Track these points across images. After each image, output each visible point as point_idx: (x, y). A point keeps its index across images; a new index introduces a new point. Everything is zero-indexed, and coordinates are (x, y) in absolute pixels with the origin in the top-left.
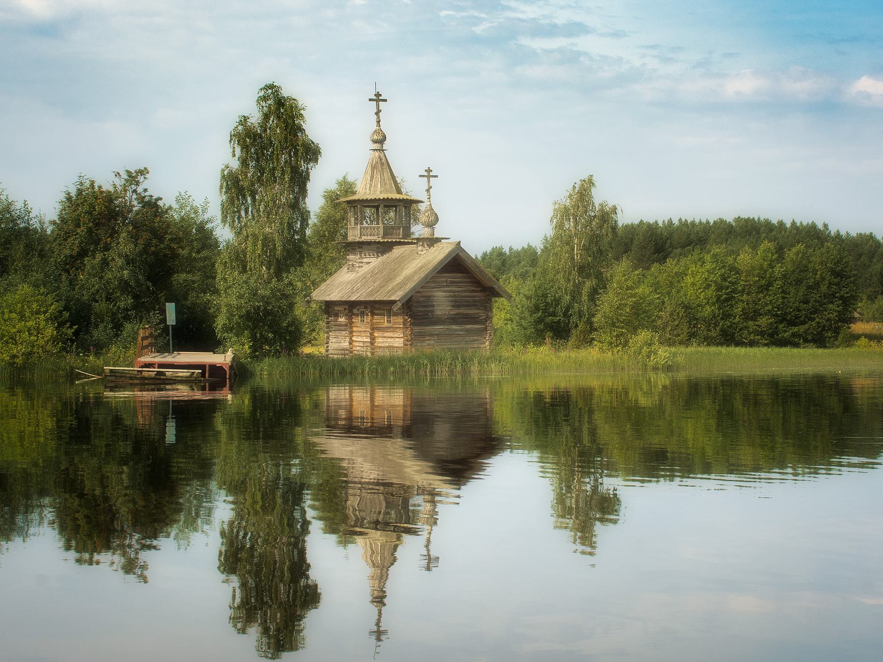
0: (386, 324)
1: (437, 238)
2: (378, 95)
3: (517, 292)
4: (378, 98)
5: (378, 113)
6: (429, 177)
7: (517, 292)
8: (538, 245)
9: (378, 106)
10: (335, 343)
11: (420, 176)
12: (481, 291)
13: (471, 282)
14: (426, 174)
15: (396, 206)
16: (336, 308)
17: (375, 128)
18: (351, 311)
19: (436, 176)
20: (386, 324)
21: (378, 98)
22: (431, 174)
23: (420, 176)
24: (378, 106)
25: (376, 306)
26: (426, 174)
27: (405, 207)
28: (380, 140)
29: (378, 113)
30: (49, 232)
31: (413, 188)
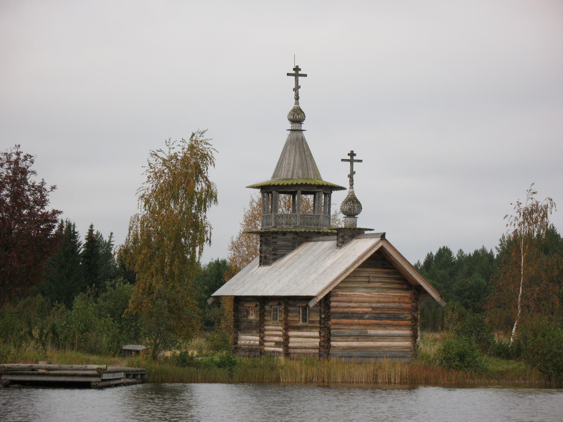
0: (301, 323)
1: (360, 229)
2: (297, 69)
3: (236, 346)
4: (297, 73)
5: (297, 88)
6: (352, 161)
7: (236, 346)
8: (493, 247)
9: (297, 81)
10: (281, 333)
11: (342, 160)
12: (406, 289)
13: (397, 279)
14: (349, 158)
15: (314, 193)
16: (247, 305)
17: (291, 105)
18: (262, 308)
19: (361, 161)
20: (301, 323)
21: (297, 73)
22: (355, 158)
23: (342, 160)
24: (297, 81)
25: (291, 302)
26: (349, 158)
27: (325, 194)
28: (297, 117)
29: (297, 88)
30: (495, 257)
31: (331, 171)
